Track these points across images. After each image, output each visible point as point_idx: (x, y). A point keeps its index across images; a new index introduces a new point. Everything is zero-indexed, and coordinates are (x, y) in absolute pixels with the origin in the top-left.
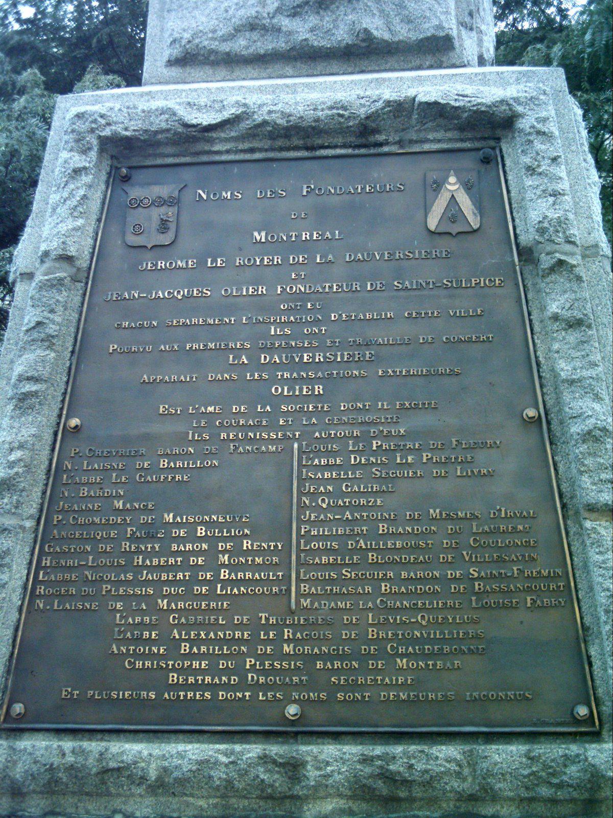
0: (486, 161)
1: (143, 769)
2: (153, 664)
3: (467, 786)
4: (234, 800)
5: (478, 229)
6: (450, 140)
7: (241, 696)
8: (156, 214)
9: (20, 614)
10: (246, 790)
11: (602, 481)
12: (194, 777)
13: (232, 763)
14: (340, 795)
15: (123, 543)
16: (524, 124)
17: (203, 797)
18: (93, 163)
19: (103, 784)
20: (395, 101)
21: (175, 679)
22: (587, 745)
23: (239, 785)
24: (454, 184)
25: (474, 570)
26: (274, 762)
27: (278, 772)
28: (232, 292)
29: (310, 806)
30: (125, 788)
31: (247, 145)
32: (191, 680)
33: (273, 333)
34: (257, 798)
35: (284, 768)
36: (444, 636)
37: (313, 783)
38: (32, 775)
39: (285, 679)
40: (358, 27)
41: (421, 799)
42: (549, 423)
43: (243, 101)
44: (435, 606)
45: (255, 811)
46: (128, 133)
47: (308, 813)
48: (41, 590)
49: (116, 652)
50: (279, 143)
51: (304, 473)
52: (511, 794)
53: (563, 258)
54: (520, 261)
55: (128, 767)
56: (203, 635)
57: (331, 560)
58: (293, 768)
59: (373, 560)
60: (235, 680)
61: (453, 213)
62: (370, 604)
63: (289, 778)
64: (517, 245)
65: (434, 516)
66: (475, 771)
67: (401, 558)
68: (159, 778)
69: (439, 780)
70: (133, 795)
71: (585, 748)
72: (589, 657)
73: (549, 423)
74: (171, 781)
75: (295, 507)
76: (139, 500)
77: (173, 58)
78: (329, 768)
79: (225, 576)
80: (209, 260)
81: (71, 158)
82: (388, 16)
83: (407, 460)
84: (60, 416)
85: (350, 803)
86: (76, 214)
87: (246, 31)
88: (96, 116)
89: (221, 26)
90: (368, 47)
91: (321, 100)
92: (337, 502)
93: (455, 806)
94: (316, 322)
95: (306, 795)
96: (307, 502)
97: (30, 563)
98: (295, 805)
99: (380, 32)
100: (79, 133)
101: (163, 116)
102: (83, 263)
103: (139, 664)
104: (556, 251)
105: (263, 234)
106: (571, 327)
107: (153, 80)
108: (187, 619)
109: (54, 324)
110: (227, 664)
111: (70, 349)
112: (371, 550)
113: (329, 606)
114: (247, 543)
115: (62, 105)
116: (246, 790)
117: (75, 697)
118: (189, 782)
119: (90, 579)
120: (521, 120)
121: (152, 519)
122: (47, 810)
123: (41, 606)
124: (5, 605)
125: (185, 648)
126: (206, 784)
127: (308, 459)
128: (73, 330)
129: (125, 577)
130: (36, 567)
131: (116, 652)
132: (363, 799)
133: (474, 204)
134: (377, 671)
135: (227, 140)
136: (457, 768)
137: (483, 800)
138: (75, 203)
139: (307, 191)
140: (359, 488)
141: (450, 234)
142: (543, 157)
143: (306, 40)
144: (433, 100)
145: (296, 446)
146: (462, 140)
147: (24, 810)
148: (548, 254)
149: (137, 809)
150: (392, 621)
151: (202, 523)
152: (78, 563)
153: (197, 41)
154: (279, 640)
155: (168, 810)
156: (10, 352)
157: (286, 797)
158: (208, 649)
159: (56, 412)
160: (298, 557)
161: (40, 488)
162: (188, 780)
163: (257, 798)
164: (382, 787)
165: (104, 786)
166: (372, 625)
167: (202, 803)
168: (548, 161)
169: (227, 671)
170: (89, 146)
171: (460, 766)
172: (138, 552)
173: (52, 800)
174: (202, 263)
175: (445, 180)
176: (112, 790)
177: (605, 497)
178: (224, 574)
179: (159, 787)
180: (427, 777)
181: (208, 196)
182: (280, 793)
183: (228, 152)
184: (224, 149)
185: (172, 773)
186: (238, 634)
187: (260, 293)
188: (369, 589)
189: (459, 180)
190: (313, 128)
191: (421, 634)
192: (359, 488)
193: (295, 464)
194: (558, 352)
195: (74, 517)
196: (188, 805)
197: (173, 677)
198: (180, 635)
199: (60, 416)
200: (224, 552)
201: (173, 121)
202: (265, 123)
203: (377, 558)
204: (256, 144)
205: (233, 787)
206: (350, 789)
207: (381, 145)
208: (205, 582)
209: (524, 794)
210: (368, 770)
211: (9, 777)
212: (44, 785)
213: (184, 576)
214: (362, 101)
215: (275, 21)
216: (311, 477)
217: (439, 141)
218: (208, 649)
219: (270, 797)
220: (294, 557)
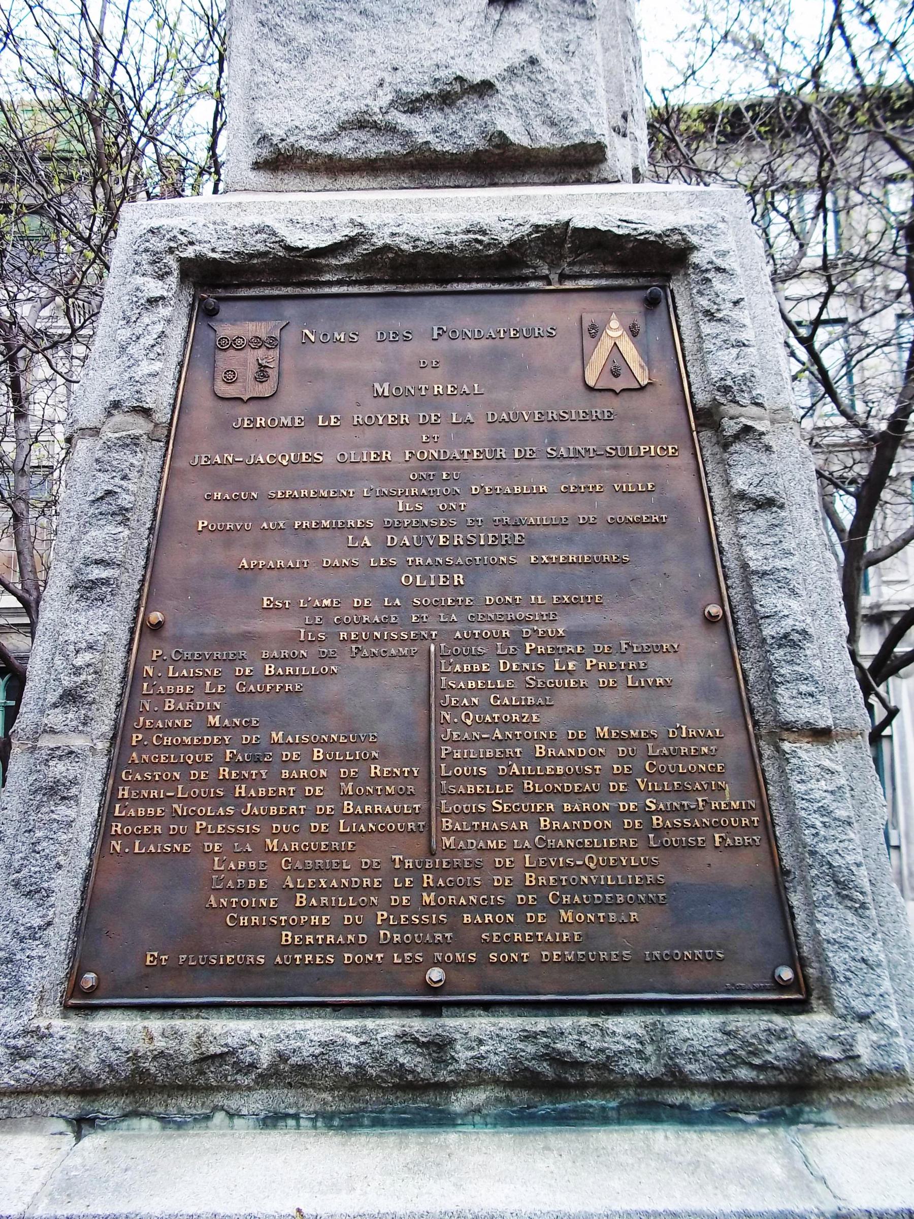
21: (289, 938)
22: (793, 1017)
27: (421, 1054)
29: (459, 1095)
32: (309, 939)
35: (428, 1049)
40: (491, 129)
42: (735, 623)
55: (233, 1052)
64: (694, 406)
68: (273, 1065)
73: (735, 623)
80: (321, 417)
86: (151, 355)
99: (518, 137)
103: (243, 921)
105: (386, 385)
120: (695, 254)
123: (118, 848)
125: (301, 899)
143: (427, 143)
144: (591, 226)
153: (292, 139)
155: (282, 1105)
159: (133, 603)
169: (354, 928)
172: (241, 779)
180: (602, 1057)
197: (287, 936)
198: (295, 883)
202: (387, 248)
214: (505, 225)
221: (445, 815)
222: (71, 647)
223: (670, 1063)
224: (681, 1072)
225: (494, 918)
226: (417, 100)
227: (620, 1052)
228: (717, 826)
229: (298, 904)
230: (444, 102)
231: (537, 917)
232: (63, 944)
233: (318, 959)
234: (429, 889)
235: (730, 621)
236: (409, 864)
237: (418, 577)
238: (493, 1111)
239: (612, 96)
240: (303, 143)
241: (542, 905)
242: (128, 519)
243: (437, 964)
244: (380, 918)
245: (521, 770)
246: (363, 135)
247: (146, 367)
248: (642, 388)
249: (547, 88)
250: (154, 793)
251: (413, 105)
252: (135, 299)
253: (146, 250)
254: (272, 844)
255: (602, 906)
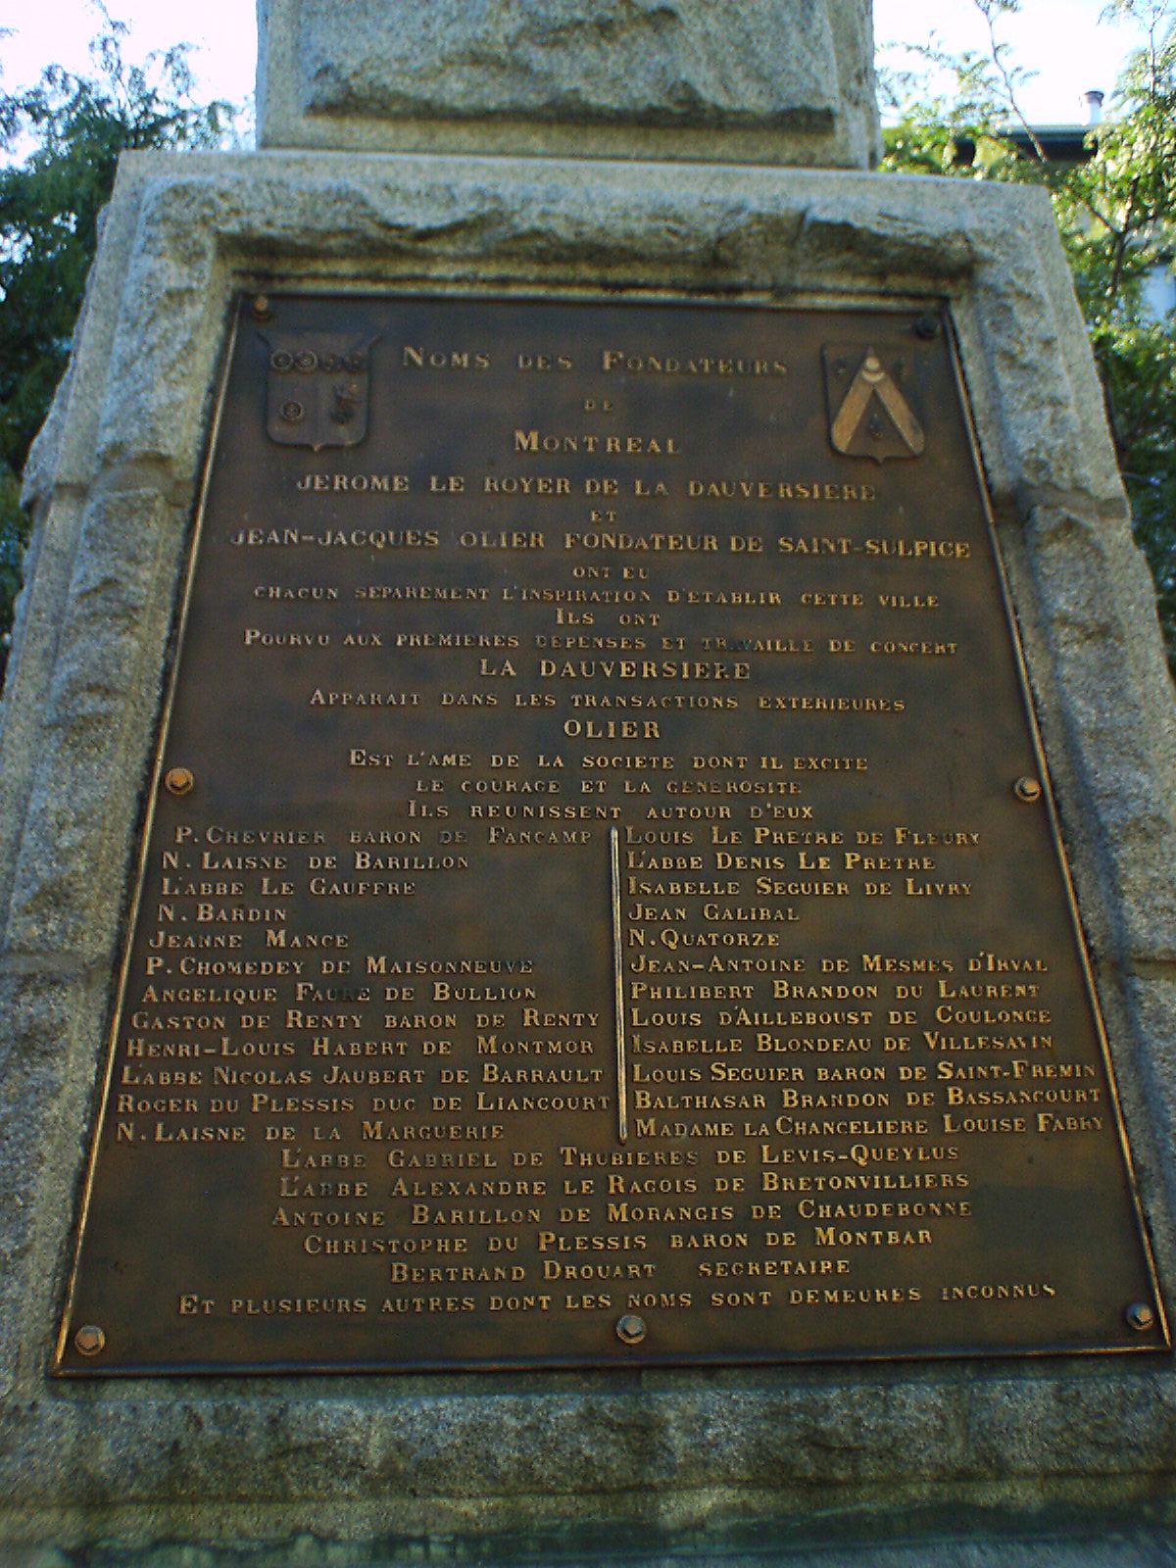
0: (923, 334)
1: (356, 1446)
2: (359, 1246)
3: (956, 1452)
4: (526, 1500)
5: (923, 454)
6: (862, 293)
7: (532, 1303)
8: (326, 385)
9: (88, 1152)
10: (554, 1477)
11: (1156, 908)
12: (459, 1459)
13: (528, 1428)
14: (729, 1482)
15: (290, 1013)
16: (988, 275)
17: (470, 1496)
18: (206, 281)
19: (276, 1479)
20: (770, 216)
21: (404, 1273)
22: (1156, 1376)
23: (544, 1470)
24: (876, 372)
25: (946, 1066)
26: (609, 1424)
27: (615, 1443)
28: (480, 541)
29: (672, 1503)
30: (320, 1484)
31: (491, 270)
32: (435, 1274)
33: (560, 621)
34: (575, 1492)
35: (625, 1434)
36: (899, 1185)
37: (681, 1460)
38: (133, 1466)
39: (613, 1269)
40: (671, 78)
41: (873, 1482)
42: (1058, 806)
43: (492, 190)
44: (880, 1131)
45: (570, 1517)
46: (273, 232)
47: (668, 1517)
48: (127, 1103)
49: (286, 1222)
50: (555, 271)
51: (632, 883)
52: (1029, 1465)
53: (1074, 516)
54: (996, 516)
55: (327, 1445)
56: (454, 1189)
57: (689, 1047)
58: (643, 1434)
59: (765, 1046)
60: (519, 1272)
61: (875, 422)
62: (764, 1129)
63: (635, 1452)
64: (990, 488)
65: (871, 966)
66: (968, 1426)
67: (815, 1044)
68: (388, 1462)
69: (908, 1446)
70: (332, 1498)
71: (1155, 1382)
72: (1147, 1219)
73: (1058, 806)
74: (411, 1467)
75: (618, 947)
76: (318, 932)
77: (320, 103)
78: (710, 1431)
79: (491, 1076)
80: (434, 480)
81: (162, 270)
82: (723, 64)
83: (818, 864)
84: (150, 764)
85: (745, 1495)
86: (173, 375)
87: (463, 64)
88: (213, 194)
89: (417, 50)
90: (685, 115)
91: (634, 200)
92: (696, 939)
93: (932, 1491)
94: (640, 606)
95: (664, 1483)
96: (641, 939)
97: (103, 1051)
98: (644, 1502)
99: (711, 94)
100: (178, 224)
101: (339, 204)
102: (185, 470)
103: (333, 1247)
104: (1063, 504)
105: (534, 436)
106: (1089, 637)
107: (282, 140)
108: (423, 1159)
109: (136, 584)
110: (504, 1243)
111: (165, 634)
112: (762, 1028)
113: (690, 1131)
114: (532, 1013)
115: (131, 169)
116: (554, 1477)
117: (207, 1311)
118: (447, 1469)
119: (227, 1081)
120: (987, 269)
121: (346, 968)
122: (160, 1534)
123: (130, 1134)
124: (57, 1132)
125: (421, 1214)
126: (480, 1471)
127: (638, 858)
128: (168, 598)
129: (298, 1077)
130: (118, 1061)
131: (286, 1222)
132: (770, 1486)
133: (911, 408)
134: (780, 1252)
135: (456, 259)
136: (938, 1423)
137: (980, 1478)
138: (173, 355)
139: (612, 364)
140: (735, 914)
141: (873, 460)
142: (1030, 339)
143: (576, 91)
144: (839, 219)
145: (615, 834)
146: (884, 295)
147: (112, 1537)
148: (1047, 507)
149: (341, 1525)
150: (804, 1159)
151: (443, 976)
152: (201, 1051)
153: (371, 74)
154: (602, 1197)
155: (402, 1525)
156: (42, 636)
157: (628, 1489)
158: (466, 1216)
159: (143, 755)
160: (629, 1041)
161: (116, 904)
162: (445, 1465)
163: (575, 1492)
164: (806, 1463)
165: (278, 1485)
166: (769, 1167)
167: (466, 1507)
168: (1037, 346)
169: (508, 1259)
170: (198, 248)
171: (943, 1418)
172: (320, 1030)
173: (169, 1515)
174: (419, 484)
175: (858, 366)
176: (295, 1490)
177: (1163, 941)
178: (490, 1072)
179: (384, 1481)
180: (887, 1440)
181: (426, 360)
182: (618, 1481)
183: (458, 280)
184: (452, 275)
185: (414, 1451)
186: (522, 1187)
187: (533, 545)
188: (760, 1100)
189: (883, 367)
190: (622, 250)
191: (858, 1181)
192: (735, 914)
193: (616, 866)
194: (1069, 681)
195: (189, 961)
196: (440, 1512)
197: (400, 1271)
198: (411, 1188)
199: (150, 764)
200: (491, 1029)
201: (362, 216)
202: (536, 233)
203: (772, 1042)
204: (508, 270)
205: (531, 1475)
206: (749, 1468)
207: (736, 290)
208: (455, 1088)
209: (1054, 1465)
210: (781, 1433)
211: (85, 1471)
212: (159, 1485)
213: (414, 1077)
214: (710, 211)
215: (519, 51)
216: (645, 892)
217: (843, 293)
218: (466, 1216)
219: (601, 1490)
220: (621, 1041)
221: (641, 1085)
222: (52, 819)
223: (984, 1445)
224: (999, 1458)
225: (717, 1240)
226: (562, 28)
227: (913, 1431)
228: (1043, 1105)
229: (416, 1221)
230: (602, 34)
231: (781, 1237)
232: (47, 1282)
233: (450, 1305)
234: (618, 1198)
235: (1050, 800)
236: (586, 1159)
237: (590, 725)
238: (721, 1525)
239: (842, 46)
240: (387, 79)
241: (790, 1219)
242: (137, 623)
243: (633, 1310)
244: (543, 1240)
245: (752, 1019)
246: (477, 74)
247: (160, 396)
248: (915, 457)
249: (751, 25)
250: (185, 1050)
251: (554, 36)
252: (145, 291)
253: (166, 219)
254: (374, 1129)
255: (878, 1222)
